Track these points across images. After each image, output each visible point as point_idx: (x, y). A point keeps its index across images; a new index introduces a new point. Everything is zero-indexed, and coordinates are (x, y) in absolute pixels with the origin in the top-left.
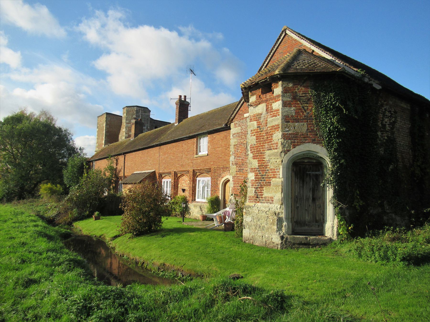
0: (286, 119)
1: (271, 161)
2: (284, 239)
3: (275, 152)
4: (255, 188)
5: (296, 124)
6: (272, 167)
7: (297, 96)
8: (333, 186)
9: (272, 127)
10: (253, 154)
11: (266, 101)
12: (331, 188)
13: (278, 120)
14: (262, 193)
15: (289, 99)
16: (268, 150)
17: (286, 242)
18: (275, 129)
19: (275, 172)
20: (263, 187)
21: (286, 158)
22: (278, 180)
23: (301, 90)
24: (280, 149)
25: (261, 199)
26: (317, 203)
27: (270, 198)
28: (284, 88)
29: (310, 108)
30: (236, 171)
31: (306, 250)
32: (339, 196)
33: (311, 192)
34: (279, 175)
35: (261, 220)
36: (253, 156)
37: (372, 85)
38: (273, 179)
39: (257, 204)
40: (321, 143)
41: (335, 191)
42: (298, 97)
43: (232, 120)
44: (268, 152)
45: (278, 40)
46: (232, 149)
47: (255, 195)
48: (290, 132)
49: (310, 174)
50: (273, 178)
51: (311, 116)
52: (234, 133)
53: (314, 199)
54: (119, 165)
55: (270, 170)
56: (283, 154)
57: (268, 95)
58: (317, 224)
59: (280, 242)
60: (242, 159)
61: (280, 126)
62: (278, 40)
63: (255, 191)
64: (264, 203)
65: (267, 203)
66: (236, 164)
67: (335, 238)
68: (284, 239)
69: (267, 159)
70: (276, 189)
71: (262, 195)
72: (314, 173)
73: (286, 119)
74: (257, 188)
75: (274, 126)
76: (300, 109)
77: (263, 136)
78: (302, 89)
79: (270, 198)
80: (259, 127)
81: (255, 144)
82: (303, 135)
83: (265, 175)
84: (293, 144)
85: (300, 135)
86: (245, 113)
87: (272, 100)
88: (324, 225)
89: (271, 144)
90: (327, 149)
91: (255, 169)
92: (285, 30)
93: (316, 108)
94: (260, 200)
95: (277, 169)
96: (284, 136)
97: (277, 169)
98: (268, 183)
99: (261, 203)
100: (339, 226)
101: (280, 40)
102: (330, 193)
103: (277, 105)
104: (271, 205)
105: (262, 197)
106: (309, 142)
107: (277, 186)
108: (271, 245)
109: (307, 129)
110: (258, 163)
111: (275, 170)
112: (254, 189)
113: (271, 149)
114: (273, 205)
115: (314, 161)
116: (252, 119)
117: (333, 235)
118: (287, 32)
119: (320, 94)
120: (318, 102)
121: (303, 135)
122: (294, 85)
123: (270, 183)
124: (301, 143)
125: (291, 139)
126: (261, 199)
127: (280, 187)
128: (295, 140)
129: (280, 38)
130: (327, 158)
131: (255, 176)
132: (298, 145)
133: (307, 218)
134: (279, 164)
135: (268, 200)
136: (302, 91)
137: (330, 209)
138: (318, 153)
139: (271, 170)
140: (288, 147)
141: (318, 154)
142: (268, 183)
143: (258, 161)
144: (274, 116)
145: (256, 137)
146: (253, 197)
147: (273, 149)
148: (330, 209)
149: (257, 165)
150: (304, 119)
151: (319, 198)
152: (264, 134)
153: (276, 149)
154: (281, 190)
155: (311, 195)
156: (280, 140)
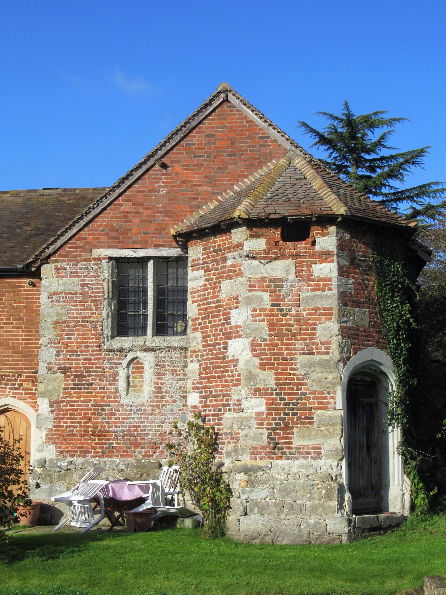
0: (343, 300)
1: (313, 376)
2: (353, 524)
3: (325, 360)
4: (268, 429)
5: (357, 310)
6: (316, 388)
7: (356, 259)
8: (402, 424)
9: (313, 309)
10: (261, 359)
11: (295, 256)
12: (397, 427)
13: (330, 299)
14: (291, 438)
15: (347, 263)
16: (304, 354)
17: (354, 527)
18: (322, 314)
19: (325, 398)
20: (292, 428)
21: (345, 372)
22: (330, 413)
23: (360, 248)
24: (335, 354)
25: (285, 450)
26: (373, 455)
27: (313, 448)
28: (340, 240)
29: (371, 283)
30: (65, 389)
31: (377, 538)
32: (408, 440)
33: (365, 435)
34: (335, 403)
35: (293, 494)
36: (260, 364)
37: (416, 251)
38: (319, 412)
39: (276, 461)
40: (386, 348)
41: (405, 432)
42: (357, 260)
43: (48, 257)
44: (301, 359)
45: (206, 105)
46: (47, 334)
47: (269, 443)
48: (349, 324)
49: (363, 401)
50: (318, 409)
51: (373, 299)
52: (53, 290)
53: (369, 448)
54: (125, 376)
55: (310, 393)
56: (341, 364)
57: (302, 246)
58: (373, 492)
59: (347, 530)
60: (84, 359)
61: (335, 311)
62: (206, 105)
63: (270, 435)
64: (298, 458)
65: (304, 458)
66: (64, 370)
67: (407, 513)
68: (353, 524)
69: (300, 372)
70: (328, 430)
71: (291, 443)
72: (367, 400)
73: (345, 300)
74: (274, 429)
75: (319, 309)
76: (360, 284)
77: (290, 325)
78: (361, 247)
79: (313, 448)
80: (278, 305)
81: (265, 340)
82: (365, 331)
83: (297, 403)
84: (353, 347)
85: (362, 331)
86: (96, 248)
87: (312, 257)
88: (383, 493)
89: (314, 344)
90: (393, 359)
91: (267, 389)
92: (226, 91)
93: (380, 284)
94: (283, 453)
95: (329, 393)
96: (345, 332)
97: (329, 393)
98: (309, 418)
99: (288, 458)
100: (415, 493)
101: (211, 108)
102: (394, 437)
103: (327, 270)
104: (315, 463)
105: (290, 448)
106: (372, 346)
107: (329, 423)
108: (326, 538)
109: (370, 322)
110: (276, 379)
111: (324, 394)
112: (266, 433)
113: (313, 354)
114: (322, 462)
115: (368, 379)
116: (255, 286)
117: (404, 509)
118: (230, 96)
119: (383, 261)
120: (382, 276)
121: (365, 331)
122: (352, 237)
123: (312, 418)
124: (363, 345)
125: (353, 337)
126: (285, 450)
127: (339, 427)
128: (355, 339)
129: (209, 104)
130: (393, 374)
131: (267, 404)
132: (360, 349)
133: (361, 483)
134: (335, 384)
135: (308, 453)
136: (362, 251)
137: (395, 463)
138: (381, 364)
139: (313, 393)
140: (347, 352)
141: (382, 367)
142: (309, 418)
143: (276, 374)
144: (318, 290)
145: (269, 325)
146: (263, 448)
147: (318, 353)
148: (395, 463)
149: (273, 382)
150: (365, 302)
151: (375, 446)
152: (292, 322)
153: (328, 353)
154: (339, 432)
155: (365, 441)
156: (335, 338)
